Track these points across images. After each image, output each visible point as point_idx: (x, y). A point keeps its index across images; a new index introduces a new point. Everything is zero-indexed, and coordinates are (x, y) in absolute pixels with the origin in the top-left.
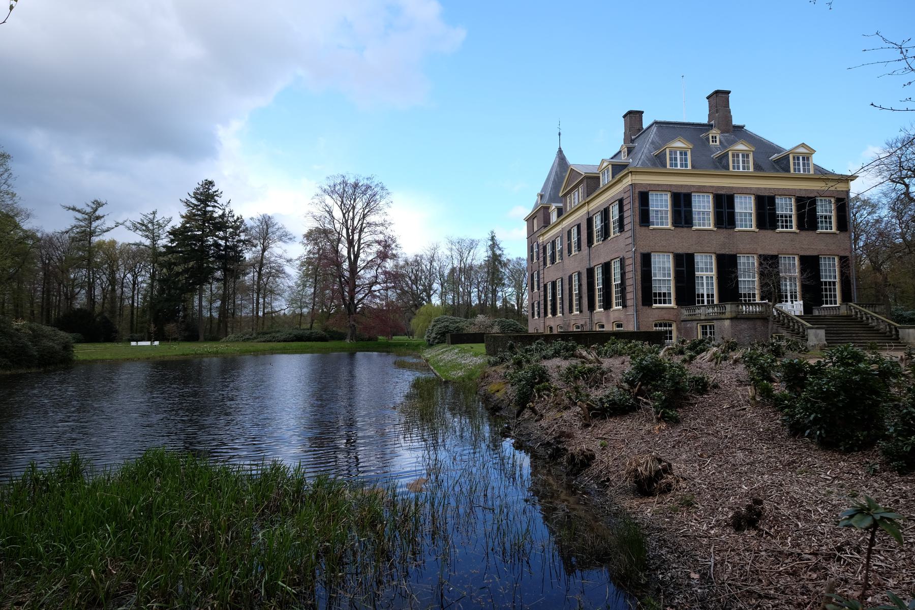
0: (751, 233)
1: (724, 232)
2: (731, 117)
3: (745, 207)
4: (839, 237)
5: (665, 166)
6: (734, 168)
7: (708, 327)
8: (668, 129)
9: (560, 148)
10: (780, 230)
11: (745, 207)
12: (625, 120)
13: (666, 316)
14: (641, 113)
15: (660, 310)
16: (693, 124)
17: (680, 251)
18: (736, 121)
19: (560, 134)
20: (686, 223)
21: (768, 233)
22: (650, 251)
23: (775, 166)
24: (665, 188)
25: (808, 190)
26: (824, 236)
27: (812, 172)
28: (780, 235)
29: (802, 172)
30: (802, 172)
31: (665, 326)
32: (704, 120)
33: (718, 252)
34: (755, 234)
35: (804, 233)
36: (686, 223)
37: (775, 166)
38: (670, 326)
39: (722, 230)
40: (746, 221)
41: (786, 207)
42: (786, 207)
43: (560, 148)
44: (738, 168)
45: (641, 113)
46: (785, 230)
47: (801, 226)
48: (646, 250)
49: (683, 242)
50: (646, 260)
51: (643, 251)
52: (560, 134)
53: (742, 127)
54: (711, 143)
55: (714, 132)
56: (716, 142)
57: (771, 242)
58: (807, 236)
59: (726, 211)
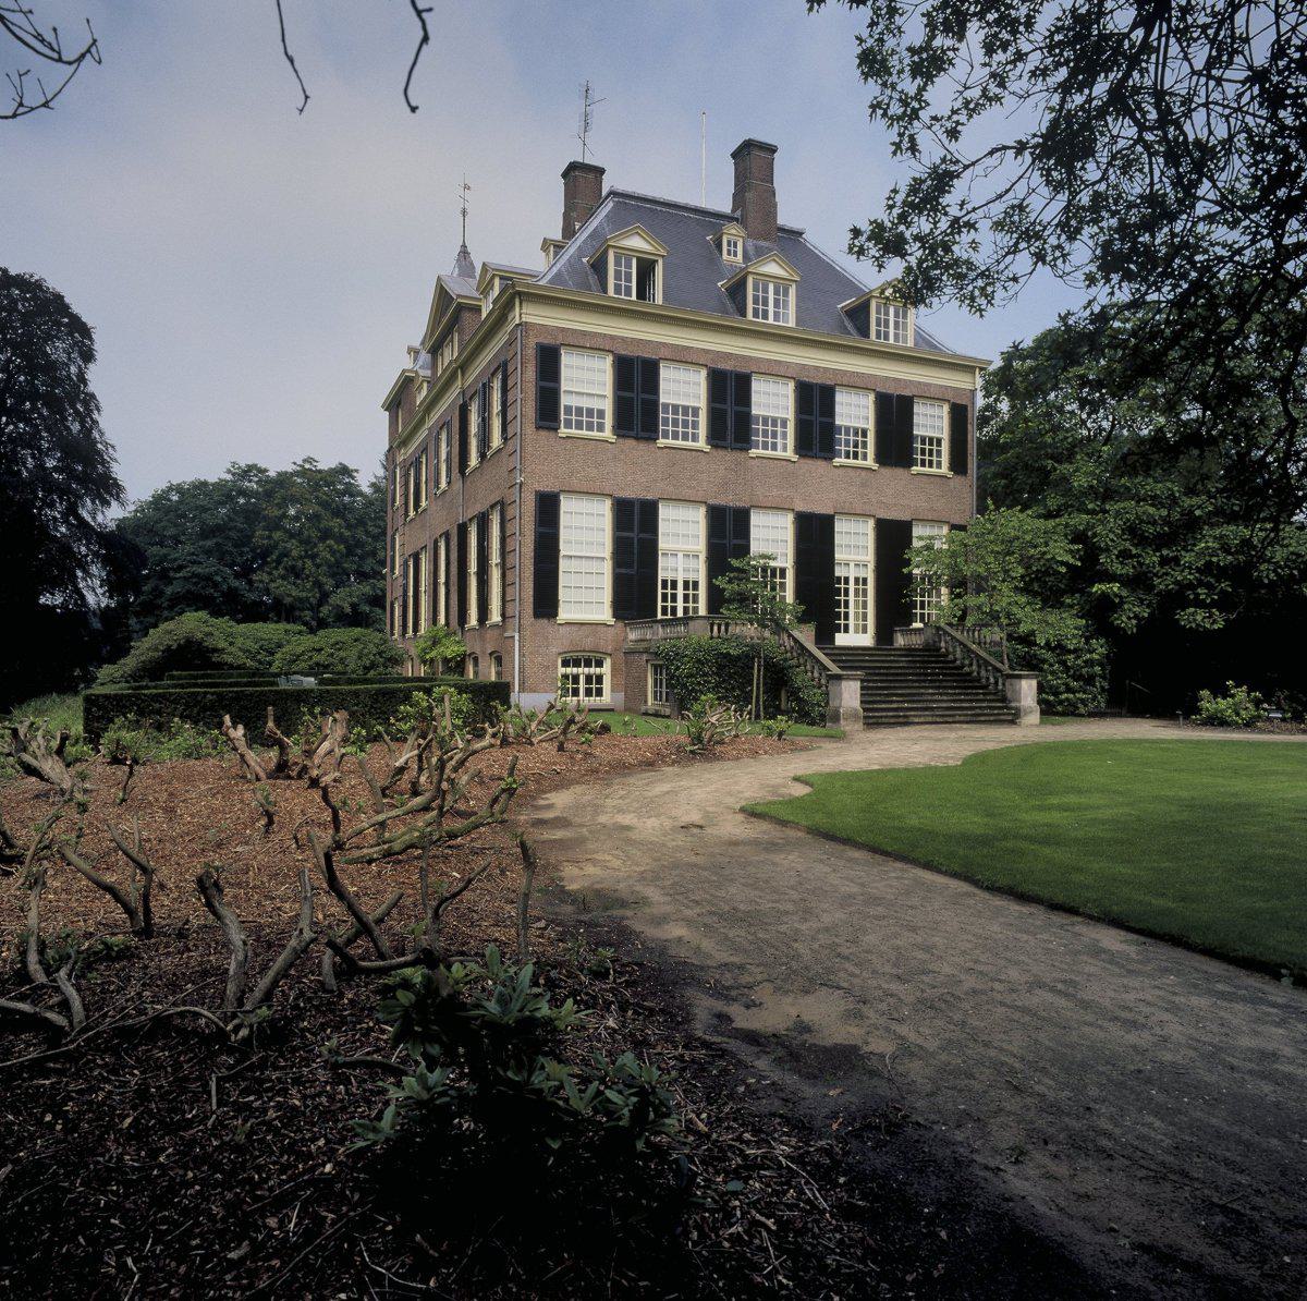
0: (784, 463)
1: (729, 457)
2: (775, 206)
3: (773, 401)
4: (951, 483)
5: (743, 313)
6: (878, 336)
7: (582, 679)
8: (638, 209)
9: (464, 246)
10: (916, 469)
11: (773, 401)
12: (565, 184)
13: (588, 643)
14: (601, 171)
15: (574, 628)
16: (696, 211)
17: (628, 494)
18: (785, 218)
19: (464, 213)
20: (737, 440)
21: (817, 467)
22: (556, 490)
23: (846, 323)
24: (600, 343)
25: (900, 380)
26: (925, 479)
27: (910, 344)
28: (840, 471)
29: (891, 341)
30: (891, 341)
31: (588, 664)
32: (726, 207)
33: (711, 502)
34: (869, 474)
35: (887, 472)
36: (737, 440)
37: (846, 323)
38: (599, 664)
39: (721, 453)
40: (774, 435)
41: (855, 412)
42: (855, 412)
43: (464, 246)
44: (765, 316)
45: (601, 171)
46: (851, 461)
47: (884, 457)
48: (547, 486)
49: (636, 471)
50: (548, 508)
51: (541, 488)
52: (464, 213)
53: (801, 234)
54: (725, 256)
55: (733, 231)
56: (735, 255)
57: (820, 486)
58: (894, 476)
59: (817, 419)
